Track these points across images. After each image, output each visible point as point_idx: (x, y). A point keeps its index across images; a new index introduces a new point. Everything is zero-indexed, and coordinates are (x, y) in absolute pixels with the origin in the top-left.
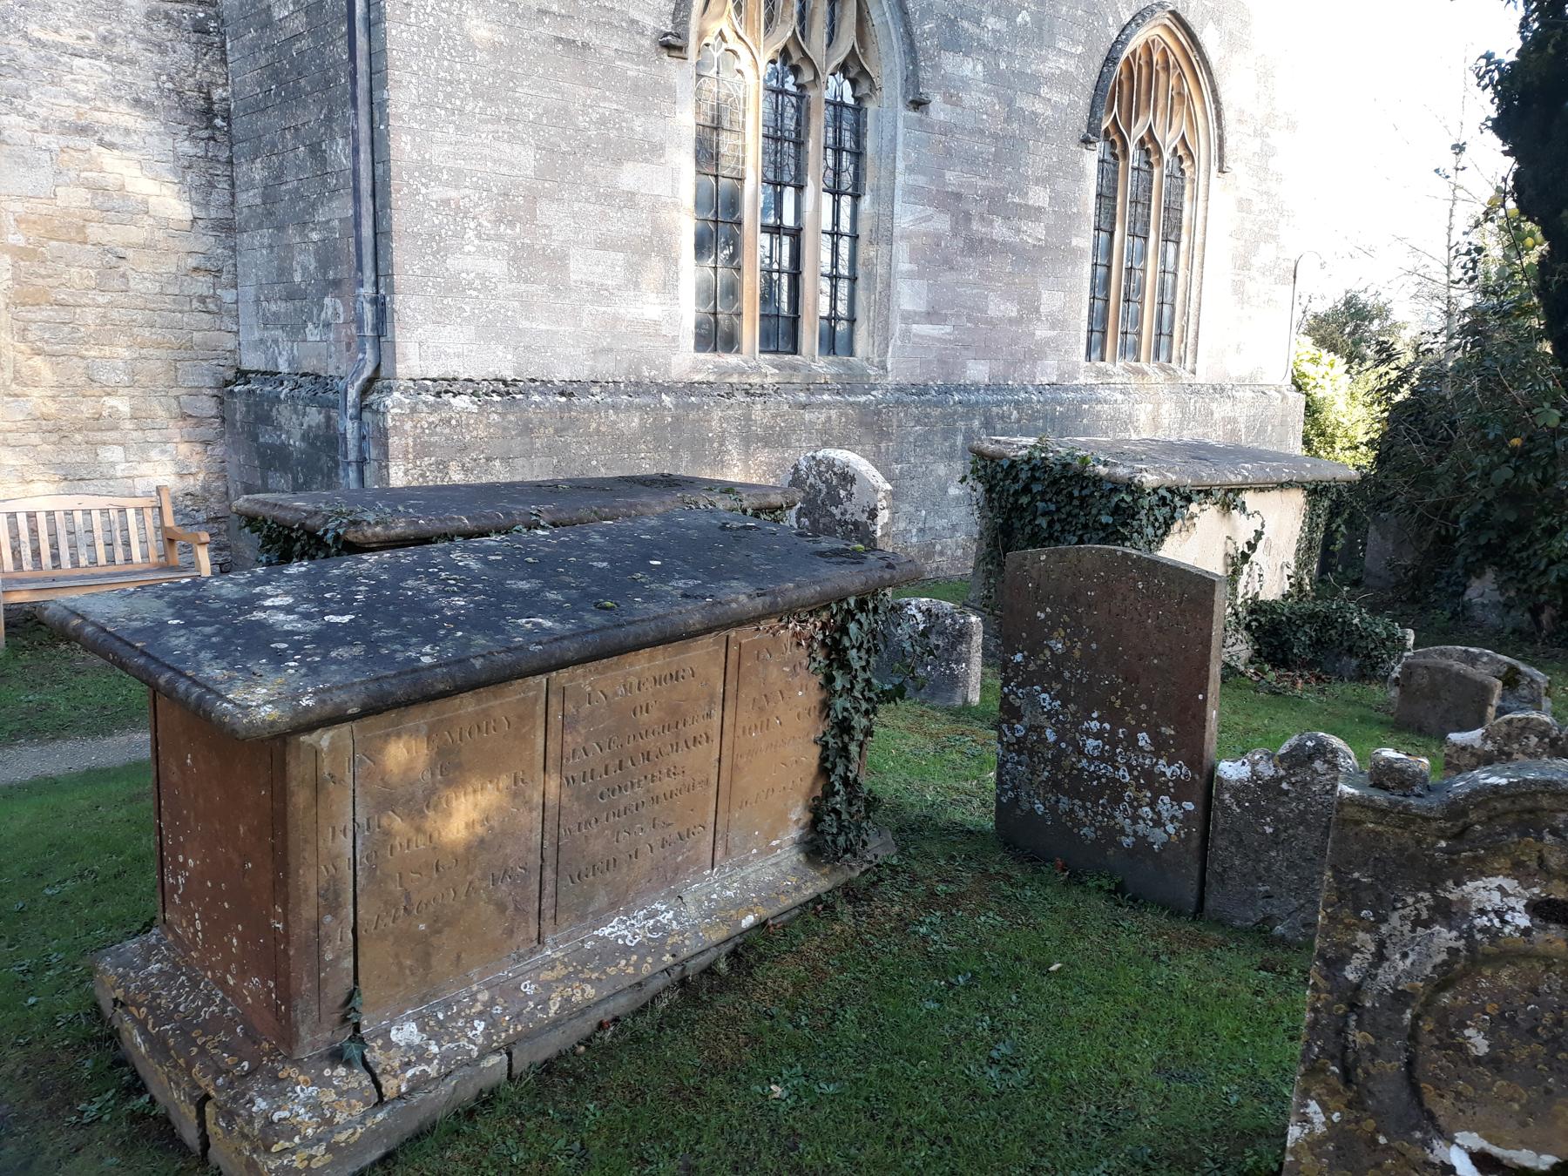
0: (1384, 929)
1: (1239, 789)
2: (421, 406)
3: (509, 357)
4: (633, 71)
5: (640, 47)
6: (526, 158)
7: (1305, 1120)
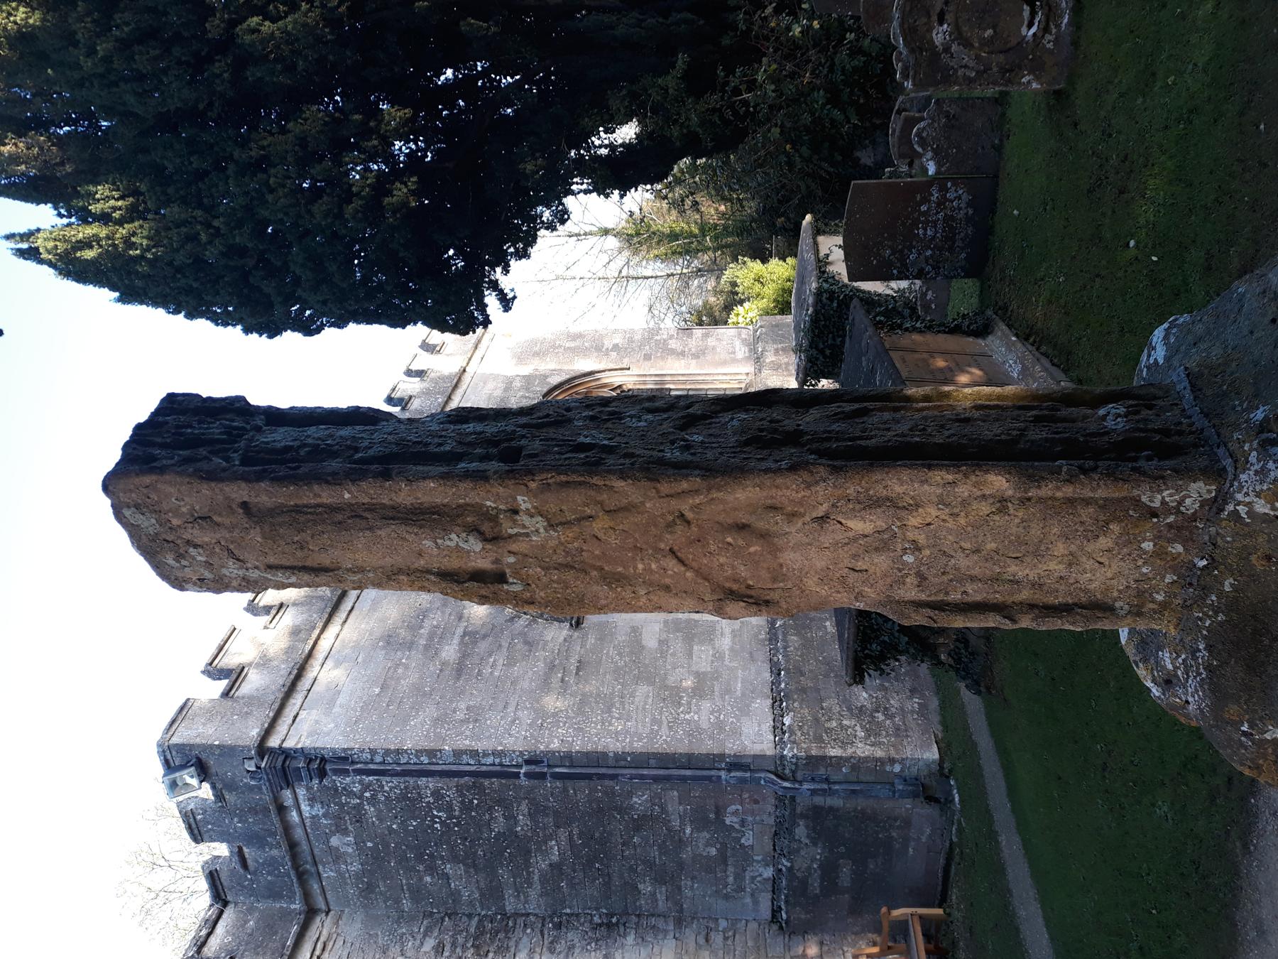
0: (956, 67)
1: (939, 165)
2: (792, 739)
3: (758, 701)
4: (591, 640)
5: (578, 637)
6: (643, 690)
7: (1029, 82)
